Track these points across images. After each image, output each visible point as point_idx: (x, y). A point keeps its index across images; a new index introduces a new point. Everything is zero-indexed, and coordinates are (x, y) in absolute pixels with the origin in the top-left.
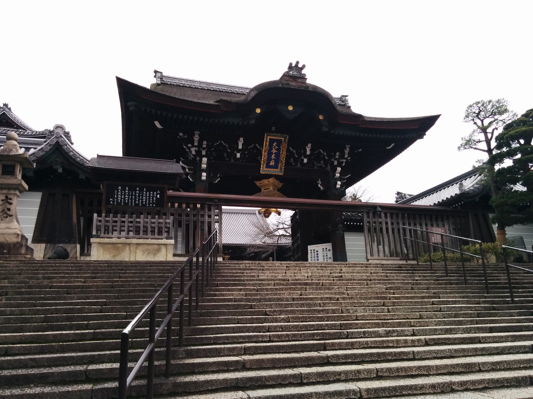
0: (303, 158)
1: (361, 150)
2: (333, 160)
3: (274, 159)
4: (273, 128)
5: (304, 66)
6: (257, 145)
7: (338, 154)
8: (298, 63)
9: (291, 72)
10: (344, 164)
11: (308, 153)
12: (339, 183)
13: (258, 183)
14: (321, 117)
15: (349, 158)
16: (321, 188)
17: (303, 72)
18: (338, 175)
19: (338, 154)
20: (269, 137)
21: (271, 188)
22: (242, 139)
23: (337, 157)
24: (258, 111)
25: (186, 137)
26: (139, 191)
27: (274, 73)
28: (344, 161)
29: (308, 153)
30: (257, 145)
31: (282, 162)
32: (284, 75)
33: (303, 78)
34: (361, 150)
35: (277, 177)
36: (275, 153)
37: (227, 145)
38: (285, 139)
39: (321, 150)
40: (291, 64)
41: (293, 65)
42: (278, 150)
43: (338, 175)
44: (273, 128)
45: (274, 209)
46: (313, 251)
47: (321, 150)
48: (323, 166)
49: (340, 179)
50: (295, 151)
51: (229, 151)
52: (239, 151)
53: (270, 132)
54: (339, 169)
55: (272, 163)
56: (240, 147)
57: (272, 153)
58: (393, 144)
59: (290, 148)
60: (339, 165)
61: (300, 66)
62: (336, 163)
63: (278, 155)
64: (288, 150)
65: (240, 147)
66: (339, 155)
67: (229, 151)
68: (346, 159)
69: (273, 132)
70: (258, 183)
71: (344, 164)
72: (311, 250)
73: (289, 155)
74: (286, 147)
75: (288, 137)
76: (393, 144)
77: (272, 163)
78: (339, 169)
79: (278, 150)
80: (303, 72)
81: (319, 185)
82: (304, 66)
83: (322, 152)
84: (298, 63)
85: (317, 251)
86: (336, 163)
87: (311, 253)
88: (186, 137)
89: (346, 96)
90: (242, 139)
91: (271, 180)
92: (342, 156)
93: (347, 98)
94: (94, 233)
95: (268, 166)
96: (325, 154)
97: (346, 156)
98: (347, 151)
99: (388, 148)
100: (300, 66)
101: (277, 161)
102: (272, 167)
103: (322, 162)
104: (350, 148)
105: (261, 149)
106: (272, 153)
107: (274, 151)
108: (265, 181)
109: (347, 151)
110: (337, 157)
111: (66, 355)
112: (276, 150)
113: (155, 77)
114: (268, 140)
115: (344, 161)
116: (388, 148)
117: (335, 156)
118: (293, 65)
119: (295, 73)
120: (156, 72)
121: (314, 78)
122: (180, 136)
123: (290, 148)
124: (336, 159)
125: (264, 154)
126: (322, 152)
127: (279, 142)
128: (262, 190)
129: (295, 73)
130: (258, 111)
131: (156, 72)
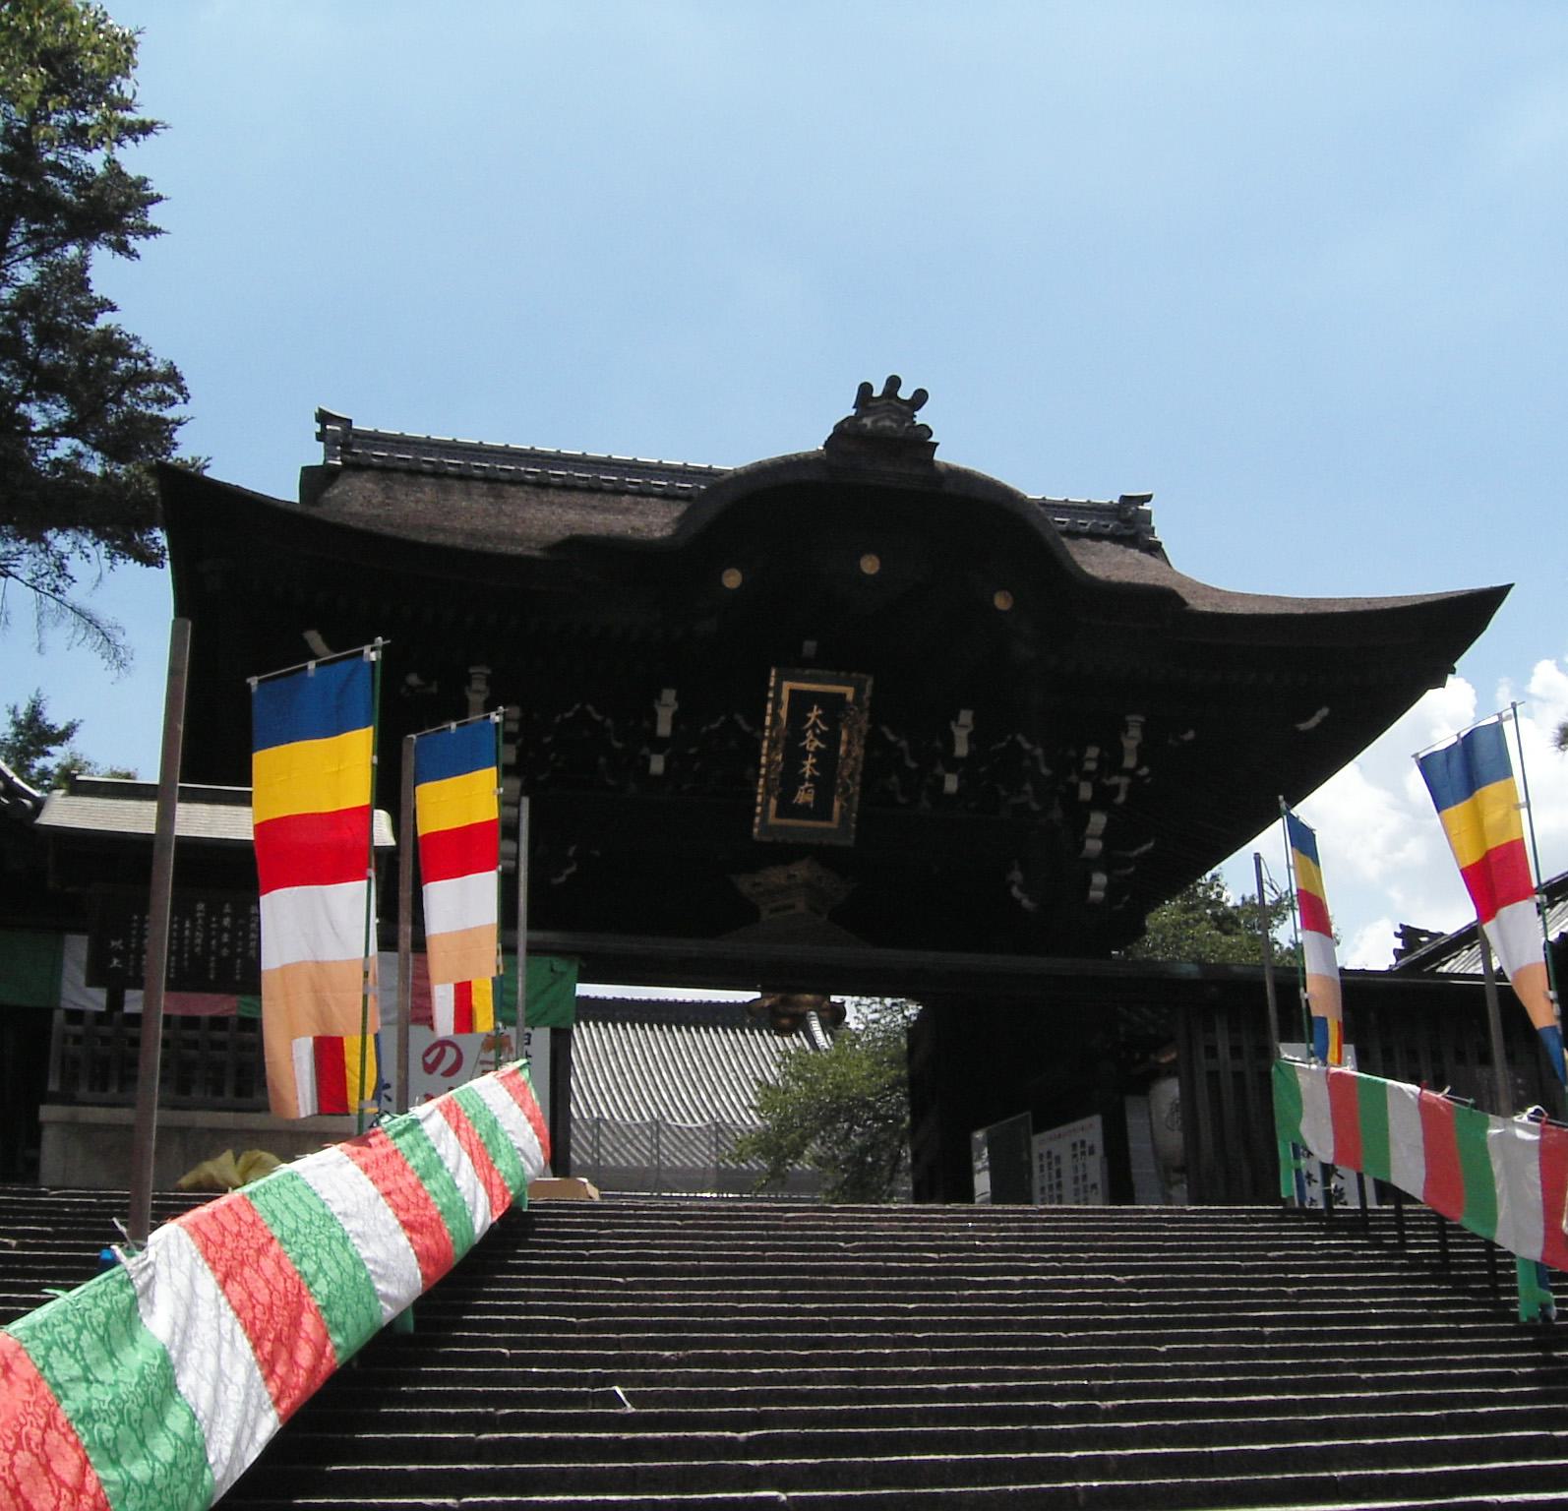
0: (939, 770)
1: (1190, 735)
2: (1073, 778)
3: (812, 778)
4: (810, 646)
5: (921, 397)
6: (738, 717)
7: (1093, 752)
8: (894, 383)
9: (868, 421)
10: (1121, 798)
11: (961, 749)
12: (1100, 879)
13: (744, 884)
14: (1002, 602)
15: (1145, 771)
16: (1026, 902)
17: (921, 417)
18: (1094, 846)
19: (1093, 752)
20: (787, 686)
21: (801, 906)
22: (669, 696)
23: (1091, 766)
24: (732, 579)
25: (434, 689)
26: (234, 917)
27: (794, 423)
28: (1124, 781)
29: (961, 749)
30: (738, 717)
31: (846, 789)
32: (843, 433)
33: (921, 442)
34: (1190, 735)
35: (824, 855)
36: (818, 753)
37: (609, 722)
38: (859, 693)
39: (1020, 738)
40: (865, 389)
41: (877, 392)
42: (831, 739)
43: (1094, 846)
44: (810, 646)
45: (809, 997)
46: (1045, 1161)
47: (1020, 738)
48: (1035, 807)
49: (1106, 862)
50: (904, 744)
51: (618, 745)
52: (659, 745)
53: (794, 664)
54: (1098, 821)
55: (804, 796)
56: (664, 728)
57: (805, 754)
58: (1325, 712)
59: (885, 729)
60: (1103, 798)
61: (905, 393)
62: (1086, 792)
63: (827, 759)
64: (873, 741)
65: (664, 728)
66: (1100, 759)
67: (618, 745)
68: (1131, 773)
69: (806, 663)
70: (744, 884)
71: (1121, 798)
72: (1041, 1156)
73: (879, 759)
74: (865, 727)
75: (870, 682)
76: (1325, 712)
77: (804, 796)
78: (1098, 821)
79: (831, 739)
80: (921, 417)
81: (1015, 891)
82: (921, 397)
83: (1027, 746)
84: (894, 383)
85: (1058, 1159)
86: (1086, 792)
87: (1042, 1170)
88: (434, 689)
89: (1147, 498)
90: (669, 696)
91: (801, 871)
92: (1112, 762)
93: (1146, 507)
94: (53, 1086)
95: (786, 808)
96: (1039, 752)
97: (1130, 762)
98: (1132, 740)
99: (1303, 726)
100: (905, 393)
101: (825, 787)
102: (803, 812)
103: (1028, 787)
104: (1144, 728)
105: (758, 734)
106: (805, 754)
107: (812, 743)
108: (776, 876)
109: (1132, 740)
110: (1091, 766)
111: (532, 1317)
112: (822, 737)
113: (320, 437)
114: (785, 697)
115: (1124, 781)
116: (1303, 726)
117: (1080, 759)
118: (877, 392)
119: (884, 432)
120: (324, 417)
121: (962, 441)
122: (411, 688)
123: (885, 729)
124: (1087, 776)
125: (769, 757)
126: (1027, 746)
127: (833, 707)
128: (765, 915)
129: (884, 432)
130: (732, 579)
131: (324, 417)
